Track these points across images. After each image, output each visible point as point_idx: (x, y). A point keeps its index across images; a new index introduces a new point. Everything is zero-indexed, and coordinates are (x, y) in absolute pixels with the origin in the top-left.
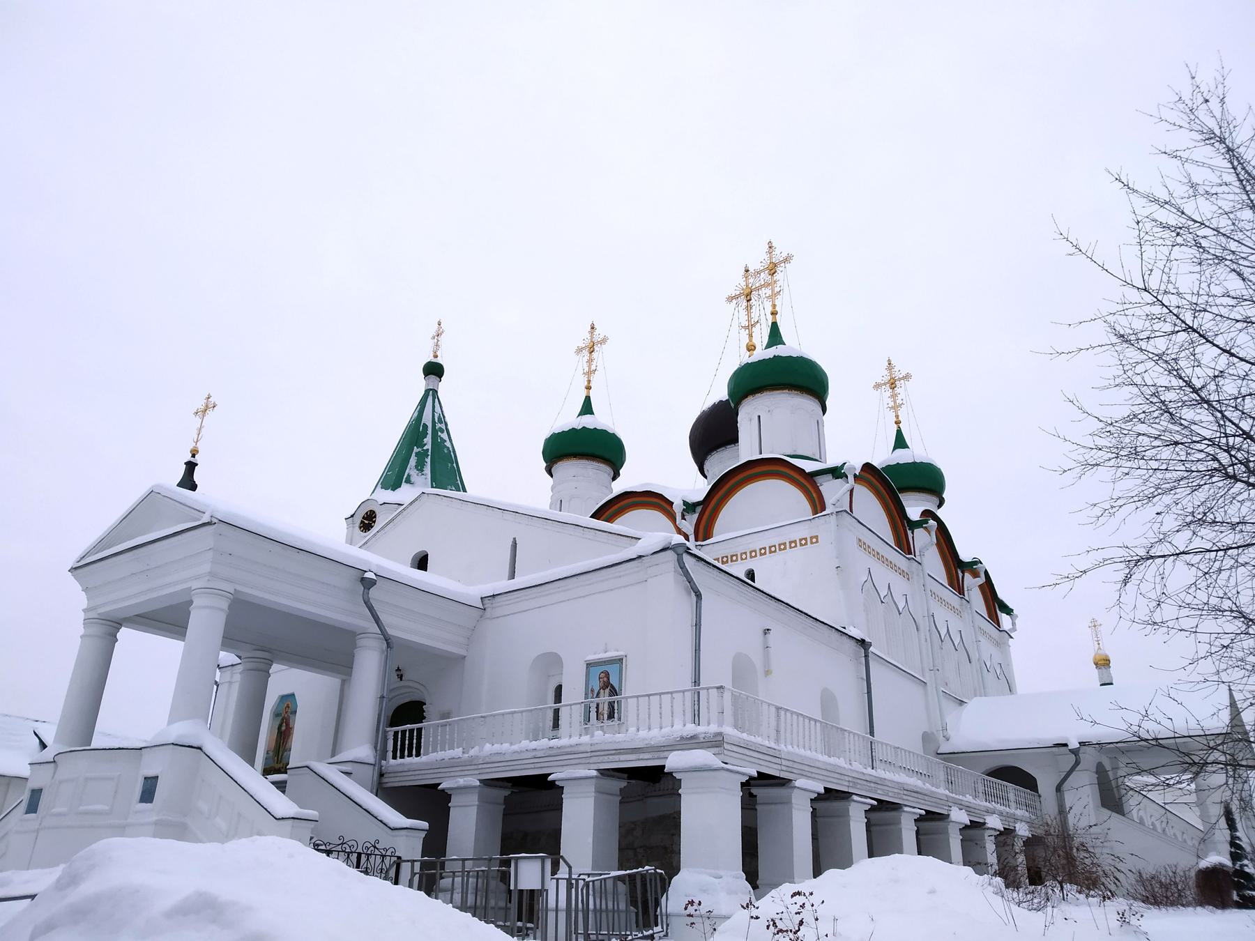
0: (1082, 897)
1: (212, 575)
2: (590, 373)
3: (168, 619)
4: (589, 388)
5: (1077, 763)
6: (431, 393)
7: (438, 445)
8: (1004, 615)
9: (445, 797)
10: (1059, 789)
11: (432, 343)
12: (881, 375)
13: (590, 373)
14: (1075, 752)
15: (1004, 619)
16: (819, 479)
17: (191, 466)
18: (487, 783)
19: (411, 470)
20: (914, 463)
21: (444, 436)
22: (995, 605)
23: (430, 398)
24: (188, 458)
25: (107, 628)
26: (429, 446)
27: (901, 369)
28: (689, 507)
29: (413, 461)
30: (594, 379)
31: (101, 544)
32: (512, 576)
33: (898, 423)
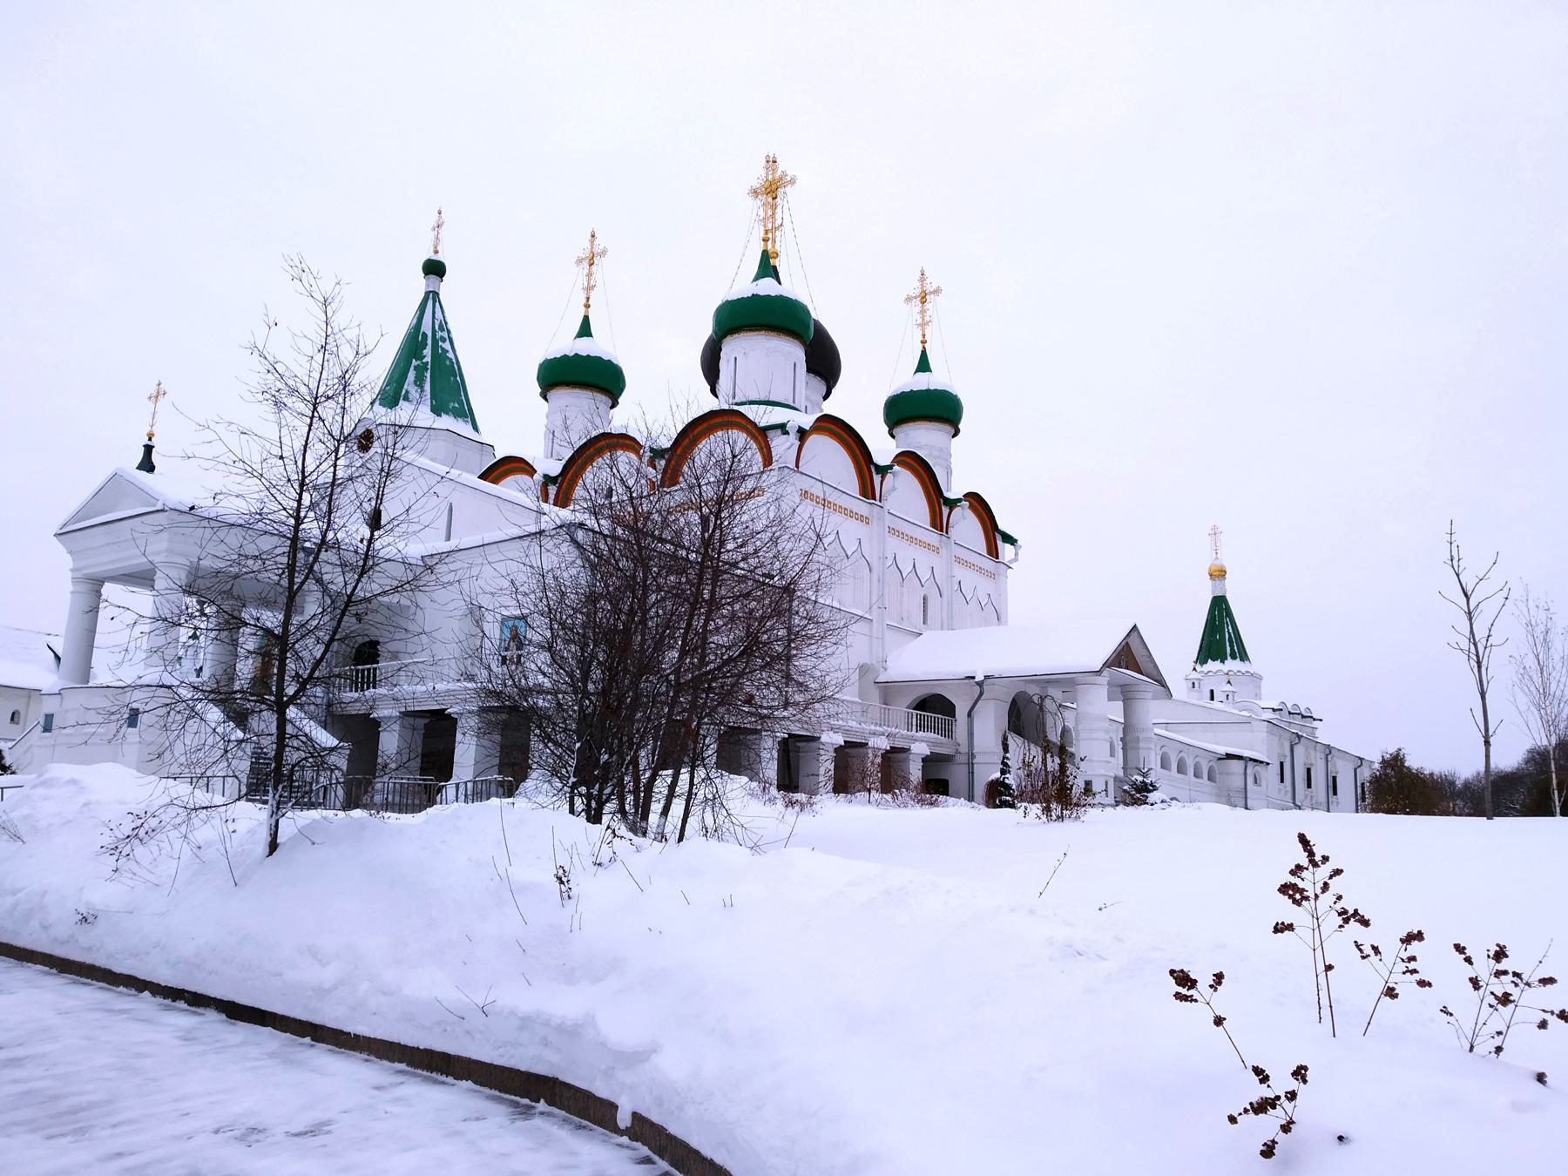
0: (888, 797)
1: (170, 551)
2: (589, 288)
3: (142, 578)
4: (587, 306)
5: (981, 694)
6: (432, 296)
7: (439, 356)
8: (1008, 546)
9: (376, 724)
10: (969, 715)
11: (432, 235)
12: (913, 288)
13: (589, 288)
14: (980, 684)
15: (1006, 550)
16: (771, 434)
17: (149, 449)
18: (406, 714)
19: (409, 385)
20: (928, 391)
21: (447, 346)
22: (995, 537)
23: (430, 303)
24: (146, 441)
25: (94, 586)
26: (428, 359)
27: (932, 282)
28: (657, 453)
29: (411, 375)
30: (593, 295)
31: (79, 515)
32: (448, 538)
33: (924, 342)
